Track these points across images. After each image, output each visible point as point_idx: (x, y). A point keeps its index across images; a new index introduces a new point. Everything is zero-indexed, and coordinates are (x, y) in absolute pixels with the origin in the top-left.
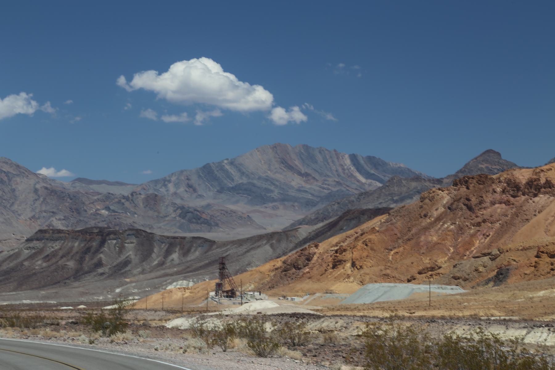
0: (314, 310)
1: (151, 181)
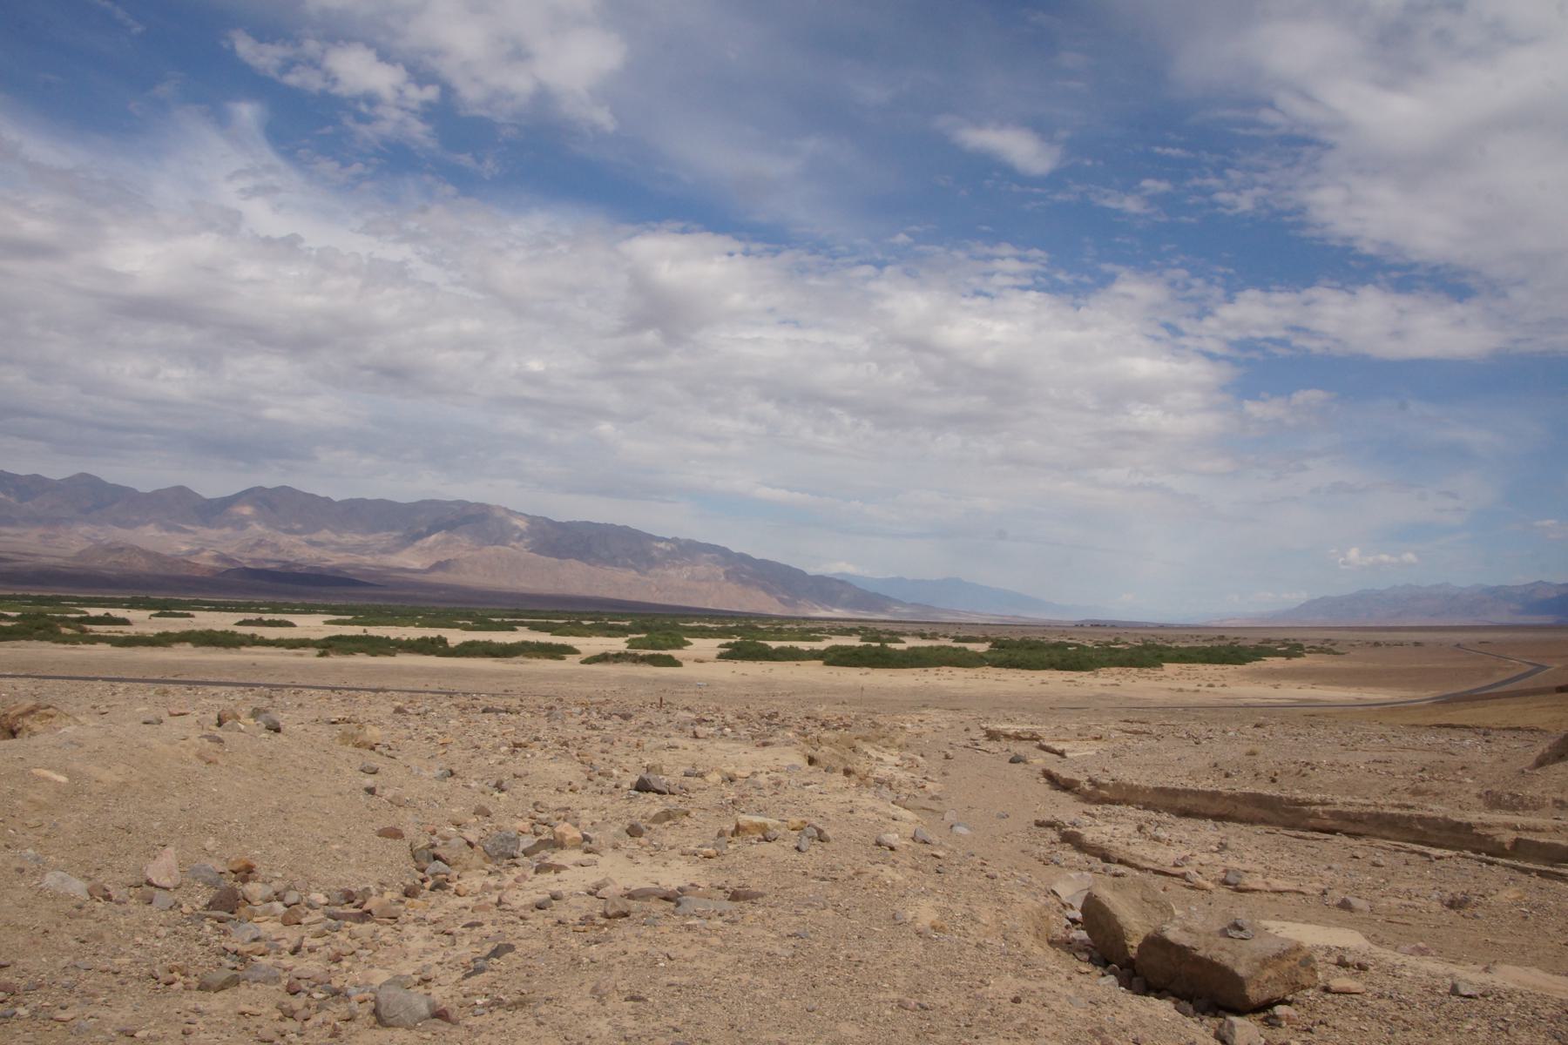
0: (528, 663)
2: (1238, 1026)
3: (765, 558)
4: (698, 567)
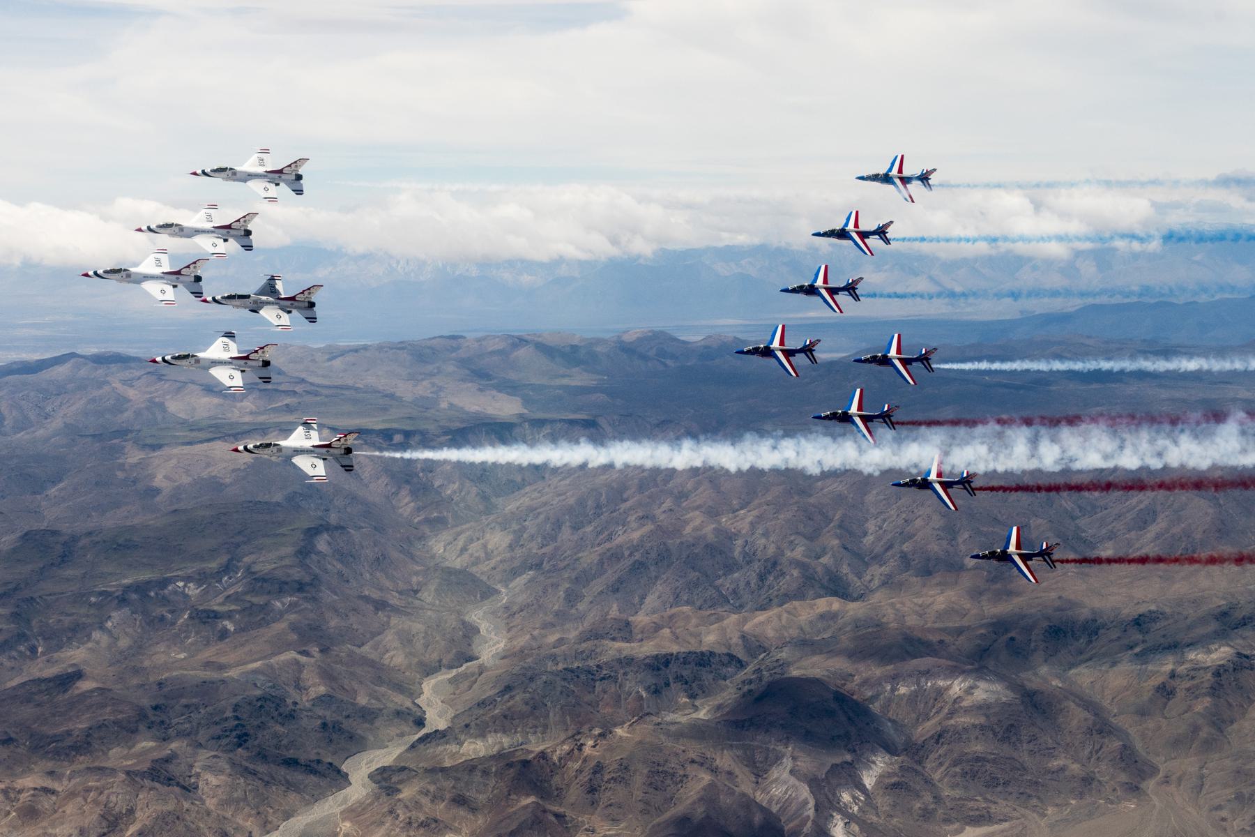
1: (401, 346)
2: (862, 295)
3: (658, 325)
4: (725, 622)
